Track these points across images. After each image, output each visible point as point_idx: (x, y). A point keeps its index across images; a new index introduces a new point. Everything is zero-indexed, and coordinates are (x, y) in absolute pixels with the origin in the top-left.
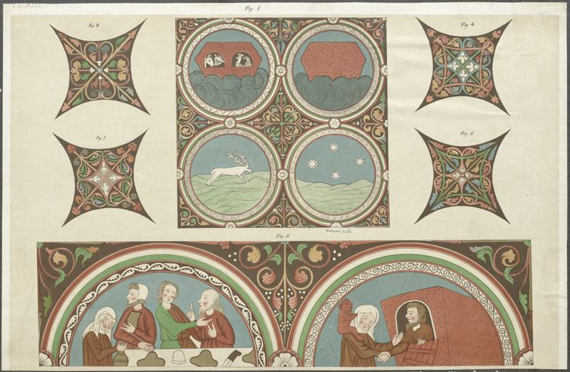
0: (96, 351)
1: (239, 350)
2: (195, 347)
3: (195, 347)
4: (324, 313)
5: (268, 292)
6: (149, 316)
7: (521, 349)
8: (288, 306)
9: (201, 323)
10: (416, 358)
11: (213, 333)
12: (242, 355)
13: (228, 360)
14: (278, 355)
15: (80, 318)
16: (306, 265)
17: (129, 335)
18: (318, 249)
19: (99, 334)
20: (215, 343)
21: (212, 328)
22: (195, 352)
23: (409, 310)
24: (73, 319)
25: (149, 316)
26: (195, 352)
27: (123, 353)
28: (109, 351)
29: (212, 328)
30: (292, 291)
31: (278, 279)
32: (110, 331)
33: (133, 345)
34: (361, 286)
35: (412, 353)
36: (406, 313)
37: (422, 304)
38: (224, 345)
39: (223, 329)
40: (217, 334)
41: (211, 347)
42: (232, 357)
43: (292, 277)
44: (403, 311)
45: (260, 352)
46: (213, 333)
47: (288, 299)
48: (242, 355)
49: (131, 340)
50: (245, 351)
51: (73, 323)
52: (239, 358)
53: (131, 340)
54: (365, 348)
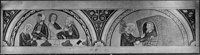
0: (25, 41)
1: (81, 40)
2: (63, 39)
3: (63, 39)
4: (112, 30)
5: (94, 22)
6: (45, 26)
7: (95, 41)
8: (100, 27)
9: (66, 30)
10: (150, 43)
11: (71, 34)
12: (82, 42)
13: (77, 44)
14: (96, 42)
15: (19, 27)
16: (104, 15)
17: (37, 34)
18: (107, 11)
19: (26, 34)
20: (71, 37)
21: (70, 32)
22: (64, 41)
23: (147, 25)
24: (16, 28)
25: (45, 26)
26: (64, 41)
27: (35, 41)
28: (29, 41)
29: (70, 32)
30: (101, 23)
31: (97, 19)
32: (30, 32)
33: (39, 38)
34: (125, 18)
35: (149, 41)
36: (147, 26)
37: (153, 22)
38: (75, 38)
39: (75, 32)
40: (73, 34)
41: (70, 39)
42: (78, 43)
43: (100, 19)
44: (145, 25)
45: (89, 41)
46: (71, 34)
47: (99, 25)
48: (82, 42)
49: (38, 36)
50: (84, 40)
51: (16, 29)
52: (81, 44)
53: (38, 36)
54: (130, 39)
